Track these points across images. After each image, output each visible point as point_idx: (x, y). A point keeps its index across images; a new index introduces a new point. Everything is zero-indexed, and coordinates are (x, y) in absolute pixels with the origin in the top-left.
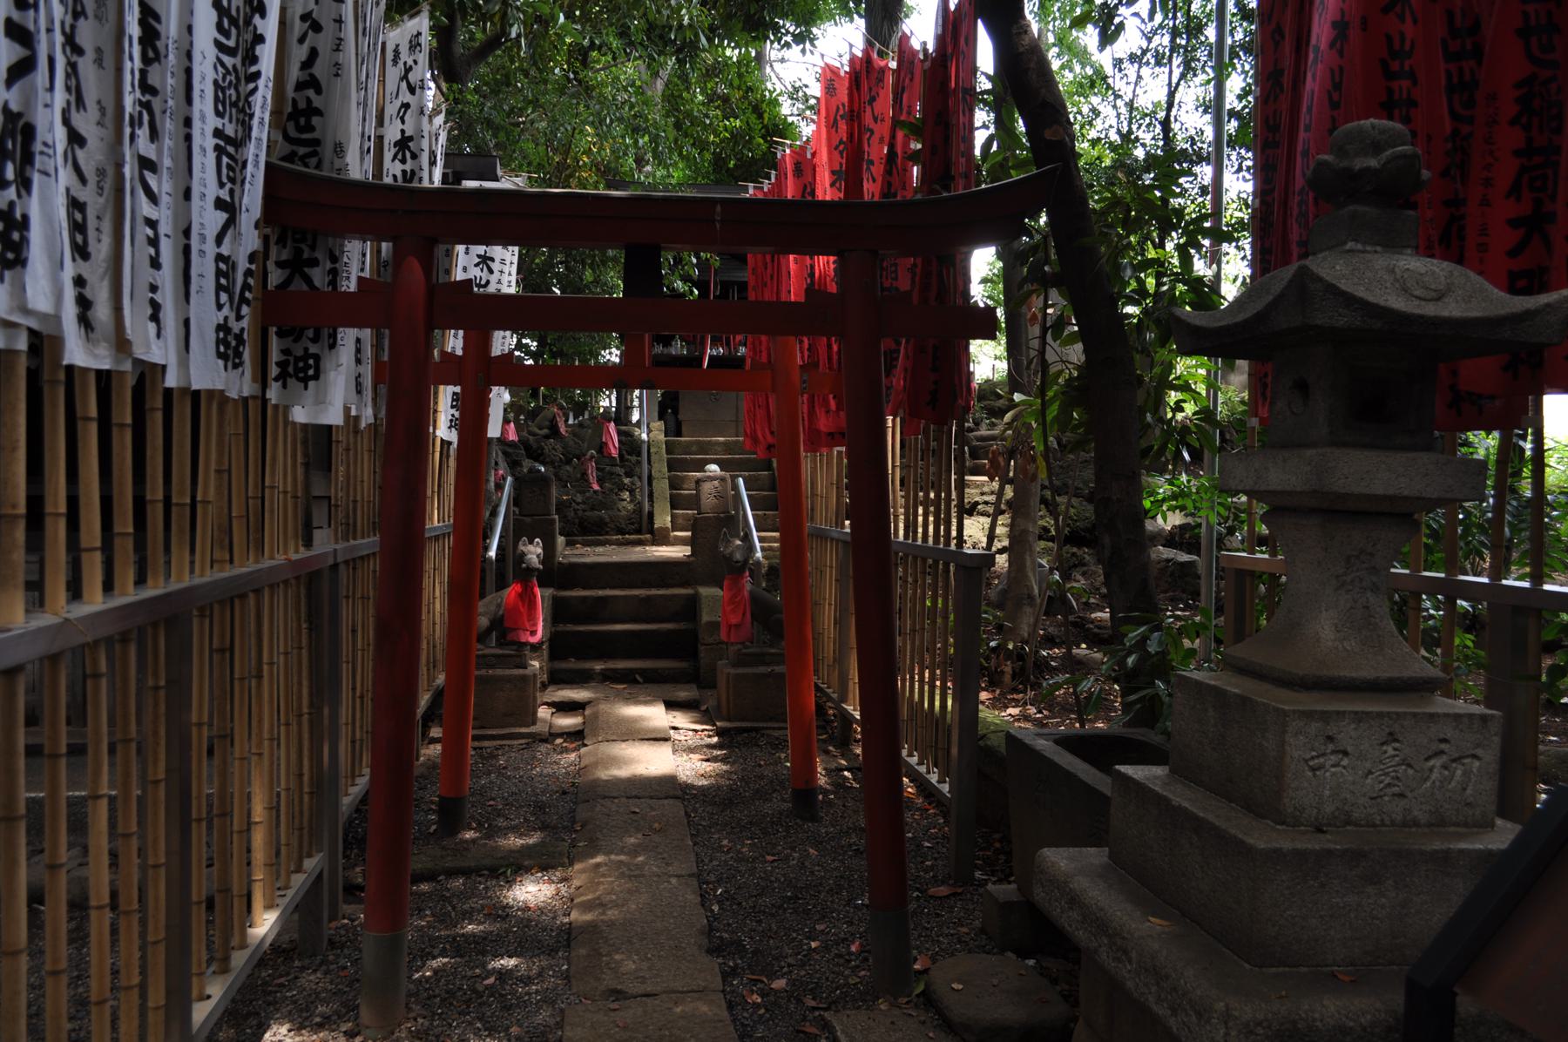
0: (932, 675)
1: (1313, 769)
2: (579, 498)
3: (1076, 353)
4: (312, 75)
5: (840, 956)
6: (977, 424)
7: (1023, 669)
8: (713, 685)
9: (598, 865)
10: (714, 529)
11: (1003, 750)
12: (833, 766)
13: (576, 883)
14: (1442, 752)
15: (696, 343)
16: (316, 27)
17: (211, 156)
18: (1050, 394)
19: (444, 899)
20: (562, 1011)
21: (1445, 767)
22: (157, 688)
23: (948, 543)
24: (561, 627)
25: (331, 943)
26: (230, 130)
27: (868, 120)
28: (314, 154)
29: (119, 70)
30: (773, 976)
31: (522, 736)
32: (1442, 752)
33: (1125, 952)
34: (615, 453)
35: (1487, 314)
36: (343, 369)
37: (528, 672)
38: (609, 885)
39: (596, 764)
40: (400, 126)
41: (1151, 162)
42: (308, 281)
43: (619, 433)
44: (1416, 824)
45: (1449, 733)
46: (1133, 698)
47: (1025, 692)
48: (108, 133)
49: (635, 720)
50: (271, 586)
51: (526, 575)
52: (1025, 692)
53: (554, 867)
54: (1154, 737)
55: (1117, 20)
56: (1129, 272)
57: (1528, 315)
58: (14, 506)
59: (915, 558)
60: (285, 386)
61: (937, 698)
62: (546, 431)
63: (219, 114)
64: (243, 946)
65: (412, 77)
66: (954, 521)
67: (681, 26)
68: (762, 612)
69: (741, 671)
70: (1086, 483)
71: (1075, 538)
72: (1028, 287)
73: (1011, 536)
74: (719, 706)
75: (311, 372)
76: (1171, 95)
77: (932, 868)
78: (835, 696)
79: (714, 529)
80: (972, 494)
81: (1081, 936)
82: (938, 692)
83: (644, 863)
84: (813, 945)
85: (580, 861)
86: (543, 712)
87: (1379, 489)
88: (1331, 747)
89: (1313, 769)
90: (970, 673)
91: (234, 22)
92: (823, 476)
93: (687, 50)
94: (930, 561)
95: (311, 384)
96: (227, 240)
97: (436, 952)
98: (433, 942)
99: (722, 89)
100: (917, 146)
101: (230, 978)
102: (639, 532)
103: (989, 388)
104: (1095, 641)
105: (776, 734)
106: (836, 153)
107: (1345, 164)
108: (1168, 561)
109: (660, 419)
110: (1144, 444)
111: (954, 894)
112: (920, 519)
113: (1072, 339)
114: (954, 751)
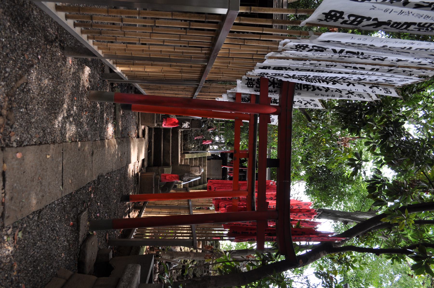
2: (193, 134)
3: (244, 269)
4: (316, 89)
9: (115, 146)
11: (140, 254)
12: (130, 205)
13: (112, 140)
15: (231, 164)
19: (111, 107)
22: (191, 58)
26: (309, 77)
27: (299, 214)
28: (298, 89)
30: (94, 193)
34: (203, 143)
39: (134, 142)
40: (297, 101)
42: (270, 86)
51: (181, 122)
53: (115, 134)
58: (247, 43)
63: (313, 76)
64: (117, 66)
65: (308, 104)
73: (185, 252)
86: (143, 127)
95: (247, 85)
98: (103, 106)
102: (184, 150)
109: (212, 155)
111: (106, 240)
113: (248, 268)
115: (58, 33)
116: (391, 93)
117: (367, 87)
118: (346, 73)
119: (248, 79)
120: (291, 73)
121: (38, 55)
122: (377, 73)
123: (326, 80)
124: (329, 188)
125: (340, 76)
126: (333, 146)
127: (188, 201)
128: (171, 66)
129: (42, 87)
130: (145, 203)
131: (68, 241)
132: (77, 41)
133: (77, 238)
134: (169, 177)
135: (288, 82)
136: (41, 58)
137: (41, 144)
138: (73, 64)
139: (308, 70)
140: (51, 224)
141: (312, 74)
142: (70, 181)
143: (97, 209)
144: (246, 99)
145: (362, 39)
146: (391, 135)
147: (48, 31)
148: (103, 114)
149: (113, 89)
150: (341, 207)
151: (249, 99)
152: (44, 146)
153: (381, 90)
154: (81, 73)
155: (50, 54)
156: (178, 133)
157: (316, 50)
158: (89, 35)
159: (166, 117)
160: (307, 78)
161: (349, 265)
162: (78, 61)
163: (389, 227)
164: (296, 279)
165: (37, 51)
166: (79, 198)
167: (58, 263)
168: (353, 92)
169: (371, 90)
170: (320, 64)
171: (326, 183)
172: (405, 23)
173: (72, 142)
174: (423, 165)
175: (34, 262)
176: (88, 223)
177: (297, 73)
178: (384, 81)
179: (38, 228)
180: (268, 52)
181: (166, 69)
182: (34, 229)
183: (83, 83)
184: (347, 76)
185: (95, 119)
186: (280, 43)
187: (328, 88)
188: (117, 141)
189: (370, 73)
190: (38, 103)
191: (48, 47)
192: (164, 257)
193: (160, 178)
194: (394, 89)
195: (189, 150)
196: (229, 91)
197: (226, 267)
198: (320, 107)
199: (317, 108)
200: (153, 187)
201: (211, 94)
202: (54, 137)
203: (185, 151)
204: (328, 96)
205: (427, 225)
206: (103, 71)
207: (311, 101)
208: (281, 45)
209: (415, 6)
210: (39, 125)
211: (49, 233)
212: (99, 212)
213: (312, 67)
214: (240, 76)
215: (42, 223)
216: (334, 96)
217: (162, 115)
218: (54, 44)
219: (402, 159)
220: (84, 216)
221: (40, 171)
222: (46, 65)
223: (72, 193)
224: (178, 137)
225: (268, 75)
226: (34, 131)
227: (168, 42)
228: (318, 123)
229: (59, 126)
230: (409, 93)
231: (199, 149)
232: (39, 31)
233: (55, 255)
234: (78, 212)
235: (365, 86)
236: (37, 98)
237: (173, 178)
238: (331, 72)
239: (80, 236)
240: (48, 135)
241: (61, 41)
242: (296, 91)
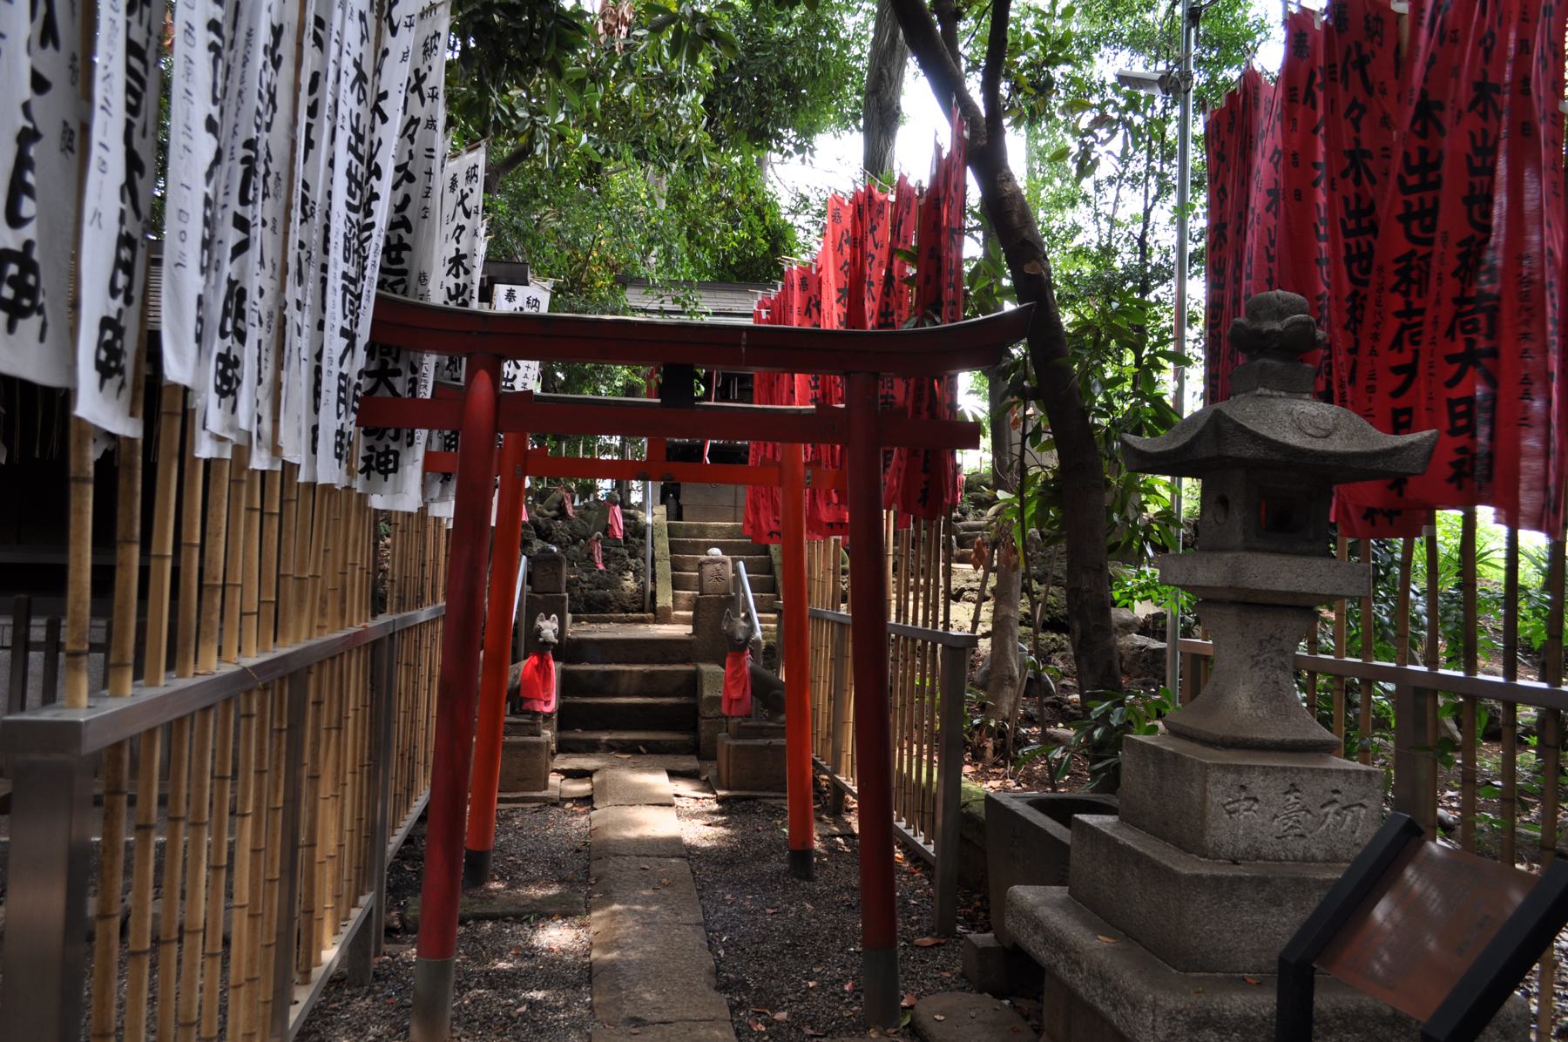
0: (920, 756)
1: (1230, 813)
2: (585, 577)
3: (1051, 459)
4: (404, 217)
5: (835, 994)
6: (964, 514)
7: (1003, 745)
8: (712, 757)
9: (614, 914)
10: (714, 609)
11: (983, 816)
12: (827, 832)
13: (594, 929)
14: (1335, 801)
16: (410, 178)
17: (340, 293)
18: (1028, 494)
19: (475, 940)
20: (589, 1034)
21: (1337, 813)
22: (280, 730)
23: (935, 626)
24: (569, 700)
25: (377, 976)
26: (352, 274)
27: (870, 247)
28: (402, 281)
29: (286, 233)
30: (775, 1009)
32: (1335, 801)
33: (1078, 963)
34: (619, 535)
35: (1364, 449)
37: (541, 739)
38: (629, 928)
41: (1129, 273)
42: (392, 388)
43: (625, 516)
44: (1314, 859)
45: (1340, 784)
46: (1098, 766)
47: (1005, 766)
49: (641, 787)
50: (359, 648)
51: (537, 646)
52: (1005, 766)
54: (1114, 801)
55: (1093, 156)
56: (1098, 389)
57: (1396, 450)
58: (216, 578)
59: (906, 639)
60: (368, 478)
61: (924, 770)
62: (554, 513)
63: (346, 260)
64: (319, 964)
66: (941, 607)
68: (762, 689)
69: (740, 742)
71: (1053, 625)
72: (1010, 399)
73: (995, 622)
74: (719, 775)
75: (391, 466)
76: (1147, 212)
77: (917, 922)
78: (828, 768)
79: (714, 609)
80: (956, 583)
81: (1043, 955)
82: (924, 765)
83: (657, 913)
84: (811, 984)
86: (554, 779)
87: (1281, 586)
88: (1244, 795)
89: (1230, 813)
90: (954, 748)
91: (359, 185)
92: (826, 564)
94: (919, 642)
95: (391, 476)
96: (347, 361)
97: (472, 984)
98: (468, 976)
99: (726, 193)
100: (911, 271)
102: (641, 610)
103: (974, 483)
104: (1069, 720)
105: (773, 802)
107: (1256, 326)
108: (1141, 647)
110: (1111, 540)
111: (938, 945)
112: (911, 604)
113: (1046, 447)
114: (939, 821)
117: (389, 41)
123: (364, 203)
125: (343, 158)
128: (315, 778)
134: (734, 686)
141: (338, 265)
145: (182, 227)
148: (499, 972)
157: (241, 314)
159: (519, 699)
168: (417, 71)
169: (402, 30)
170: (302, 245)
181: (326, 787)
184: (344, 136)
188: (601, 905)
193: (736, 721)
199: (481, 172)
200: (769, 747)
201: (429, 555)
203: (647, 606)
204: (430, 173)
208: (221, 450)
209: (50, 47)
212: (838, 981)
213: (312, 273)
214: (354, 499)
217: (513, 713)
228: (545, 129)
231: (641, 551)
235: (386, 53)
237: (736, 672)
238: (329, 194)
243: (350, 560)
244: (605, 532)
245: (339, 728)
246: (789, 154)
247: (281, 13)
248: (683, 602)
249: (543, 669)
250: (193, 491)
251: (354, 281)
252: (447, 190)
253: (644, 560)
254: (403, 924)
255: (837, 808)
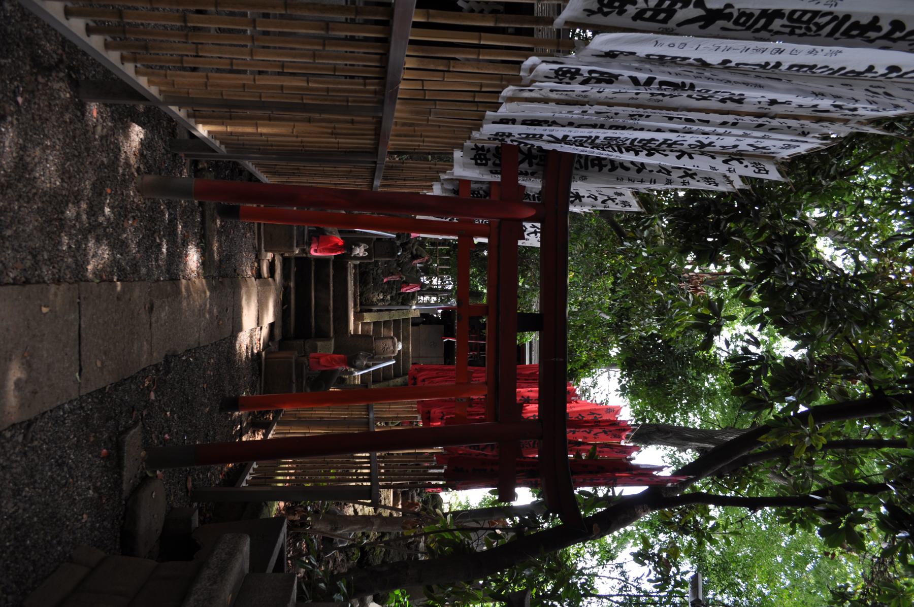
0: (290, 475)
2: (380, 271)
5: (163, 428)
7: (296, 526)
9: (205, 293)
11: (262, 517)
12: (243, 419)
13: (197, 281)
17: (588, 135)
18: (457, 533)
22: (348, 101)
24: (313, 263)
26: (598, 141)
27: (596, 430)
28: (581, 167)
30: (156, 393)
31: (260, 244)
33: (215, 583)
34: (403, 290)
36: (480, 176)
38: (197, 301)
40: (586, 195)
42: (522, 162)
43: (414, 293)
48: (602, 100)
49: (267, 306)
51: (350, 244)
53: (204, 269)
55: (646, 562)
60: (472, 149)
62: (415, 252)
63: (605, 138)
64: (197, 123)
67: (630, 325)
68: (326, 377)
70: (392, 559)
73: (364, 516)
85: (207, 282)
86: (270, 255)
93: (616, 329)
95: (473, 162)
96: (550, 138)
98: (174, 208)
101: (186, 119)
102: (361, 304)
106: (577, 415)
109: (421, 314)
110: (434, 587)
111: (187, 491)
113: (489, 544)
115: (64, 50)
116: (767, 172)
117: (719, 160)
118: (672, 131)
119: (477, 148)
120: (559, 132)
121: (15, 96)
122: (735, 131)
123: (632, 147)
124: (667, 380)
125: (660, 137)
126: (671, 293)
127: (368, 409)
128: (309, 120)
129: (28, 163)
130: (277, 413)
131: (96, 489)
132: (107, 72)
133: (118, 483)
135: (554, 151)
136: (23, 103)
137: (27, 282)
138: (102, 117)
139: (594, 126)
140: (55, 451)
141: (602, 134)
142: (99, 364)
143: (165, 425)
144: (481, 192)
145: (677, 45)
146: (779, 263)
147: (40, 46)
149: (196, 171)
150: (695, 420)
151: (487, 193)
152: (34, 288)
153: (746, 166)
154: (121, 138)
155: (46, 94)
156: (346, 269)
157: (599, 81)
158: (125, 53)
159: (318, 235)
160: (592, 142)
161: (703, 536)
162: (112, 112)
163: (785, 454)
164: (600, 571)
165: (13, 87)
166: (122, 400)
167: (74, 533)
168: (695, 174)
169: (726, 166)
170: (616, 114)
171: (660, 370)
172: (764, 13)
173: (102, 281)
174: (845, 323)
175: (18, 529)
176: (143, 454)
177: (573, 133)
178: (751, 149)
179: (24, 459)
180: (504, 87)
181: (301, 127)
182: (16, 461)
183: (127, 158)
184: (673, 137)
185: (156, 235)
186: (523, 66)
187: (642, 164)
189: (721, 130)
190: (20, 196)
191: (40, 79)
192: (317, 526)
194: (775, 164)
195: (373, 304)
196: (443, 176)
197: (442, 542)
198: (635, 207)
199: (628, 209)
201: (408, 183)
202: (60, 270)
204: (642, 181)
205: (861, 449)
206: (173, 134)
207: (615, 197)
208: (525, 70)
210: (24, 244)
211: (50, 470)
212: (170, 430)
213: (601, 120)
214: (461, 142)
215: (34, 449)
216: (655, 182)
218: (54, 74)
219: (802, 312)
220: (134, 438)
221: (26, 339)
222: (37, 118)
223: (105, 388)
224: (346, 276)
225: (512, 138)
226: (12, 255)
227: (292, 68)
229: (70, 247)
230: (817, 174)
231: (394, 303)
232: (18, 46)
233: (66, 516)
234: (120, 429)
235: (713, 158)
236: (17, 186)
238: (642, 129)
239: (125, 478)
240: (45, 264)
241: (70, 68)
242: (575, 172)
243: (426, 139)
244: (405, 282)
245: (332, 134)
246: (620, 381)
247: (748, 103)
248: (367, 327)
249: (336, 248)
250: (508, 55)
251: (593, 141)
252: (615, 190)
253: (389, 305)
254: (199, 170)
255: (255, 426)
